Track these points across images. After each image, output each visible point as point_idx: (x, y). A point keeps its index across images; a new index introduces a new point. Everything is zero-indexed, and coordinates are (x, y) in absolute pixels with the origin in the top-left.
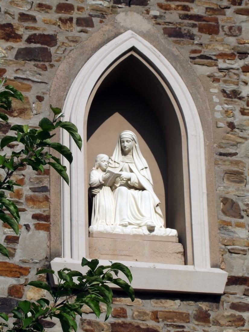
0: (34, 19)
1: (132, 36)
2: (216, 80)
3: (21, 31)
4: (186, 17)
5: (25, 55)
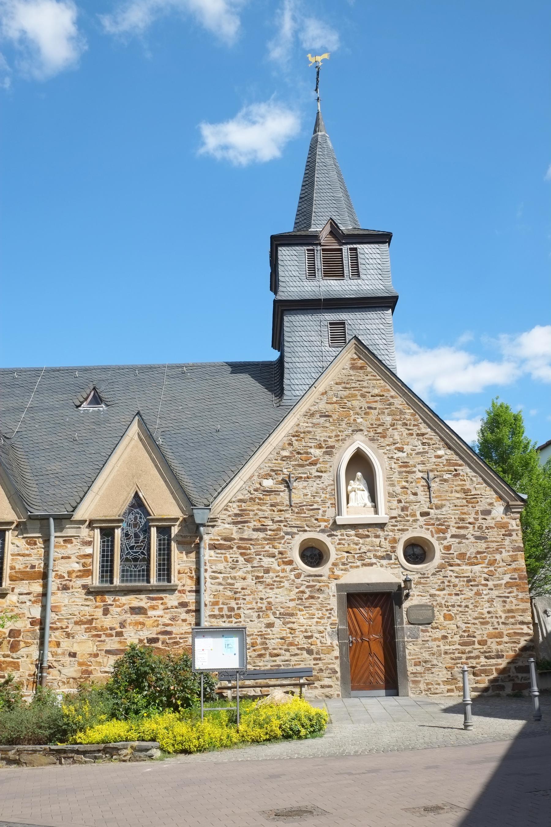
0: (328, 441)
1: (360, 442)
2: (385, 454)
3: (324, 446)
4: (376, 433)
5: (326, 453)
